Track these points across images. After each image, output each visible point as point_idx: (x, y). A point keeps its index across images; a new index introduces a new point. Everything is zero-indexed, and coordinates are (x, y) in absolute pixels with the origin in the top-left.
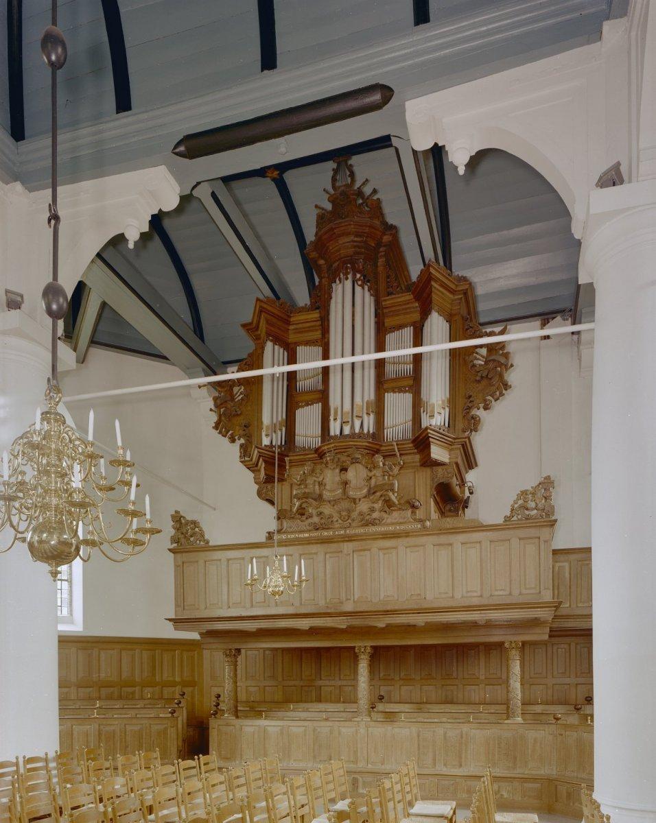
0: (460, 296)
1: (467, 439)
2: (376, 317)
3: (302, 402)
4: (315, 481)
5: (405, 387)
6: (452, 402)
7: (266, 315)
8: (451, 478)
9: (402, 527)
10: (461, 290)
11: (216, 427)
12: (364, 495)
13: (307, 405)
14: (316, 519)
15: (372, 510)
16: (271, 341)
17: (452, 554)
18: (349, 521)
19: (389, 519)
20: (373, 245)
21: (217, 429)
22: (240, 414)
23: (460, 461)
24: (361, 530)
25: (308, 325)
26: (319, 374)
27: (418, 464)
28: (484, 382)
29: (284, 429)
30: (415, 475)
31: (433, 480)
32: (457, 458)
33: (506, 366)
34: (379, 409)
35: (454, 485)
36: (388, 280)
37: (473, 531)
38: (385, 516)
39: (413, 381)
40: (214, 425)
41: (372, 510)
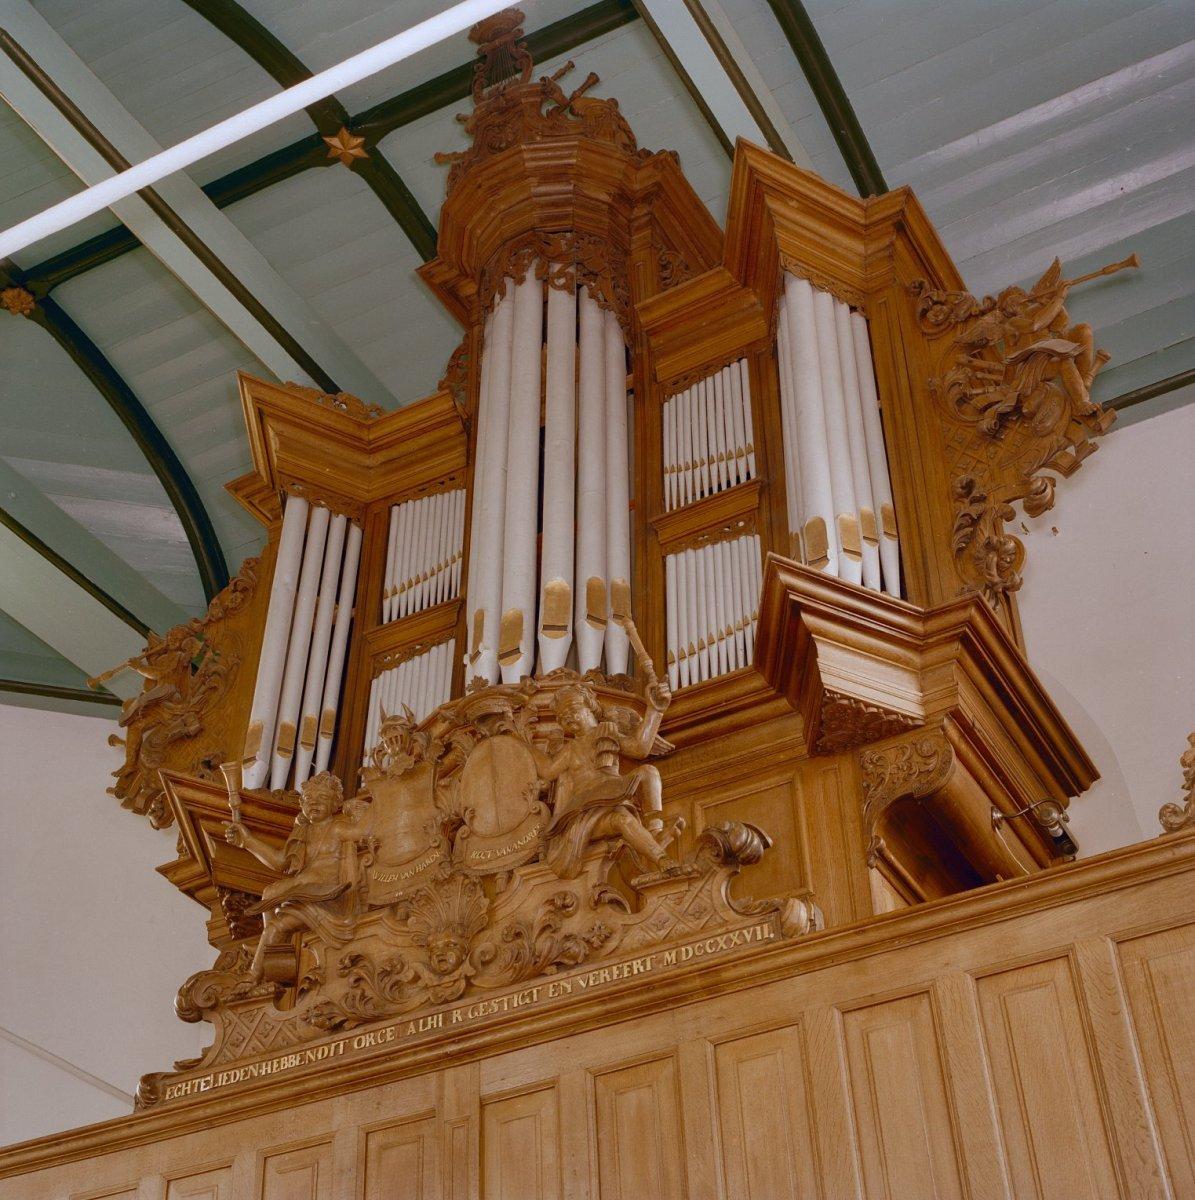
0: (886, 241)
1: (973, 611)
2: (629, 368)
3: (392, 649)
4: (343, 841)
5: (737, 518)
6: (904, 519)
7: (280, 427)
8: (943, 770)
9: (688, 952)
10: (884, 219)
11: (119, 792)
12: (526, 854)
13: (409, 653)
14: (336, 989)
15: (561, 908)
16: (299, 494)
17: (937, 1027)
18: (466, 969)
19: (633, 930)
20: (604, 197)
21: (119, 796)
22: (201, 730)
23: (969, 705)
24: (514, 1001)
25: (424, 440)
26: (454, 561)
27: (804, 750)
28: (1013, 435)
29: (325, 745)
30: (793, 794)
31: (863, 793)
32: (954, 693)
33: (1080, 360)
34: (647, 605)
35: (986, 826)
36: (666, 274)
37: (1016, 906)
38: (615, 919)
39: (761, 501)
40: (114, 782)
41: (561, 908)
